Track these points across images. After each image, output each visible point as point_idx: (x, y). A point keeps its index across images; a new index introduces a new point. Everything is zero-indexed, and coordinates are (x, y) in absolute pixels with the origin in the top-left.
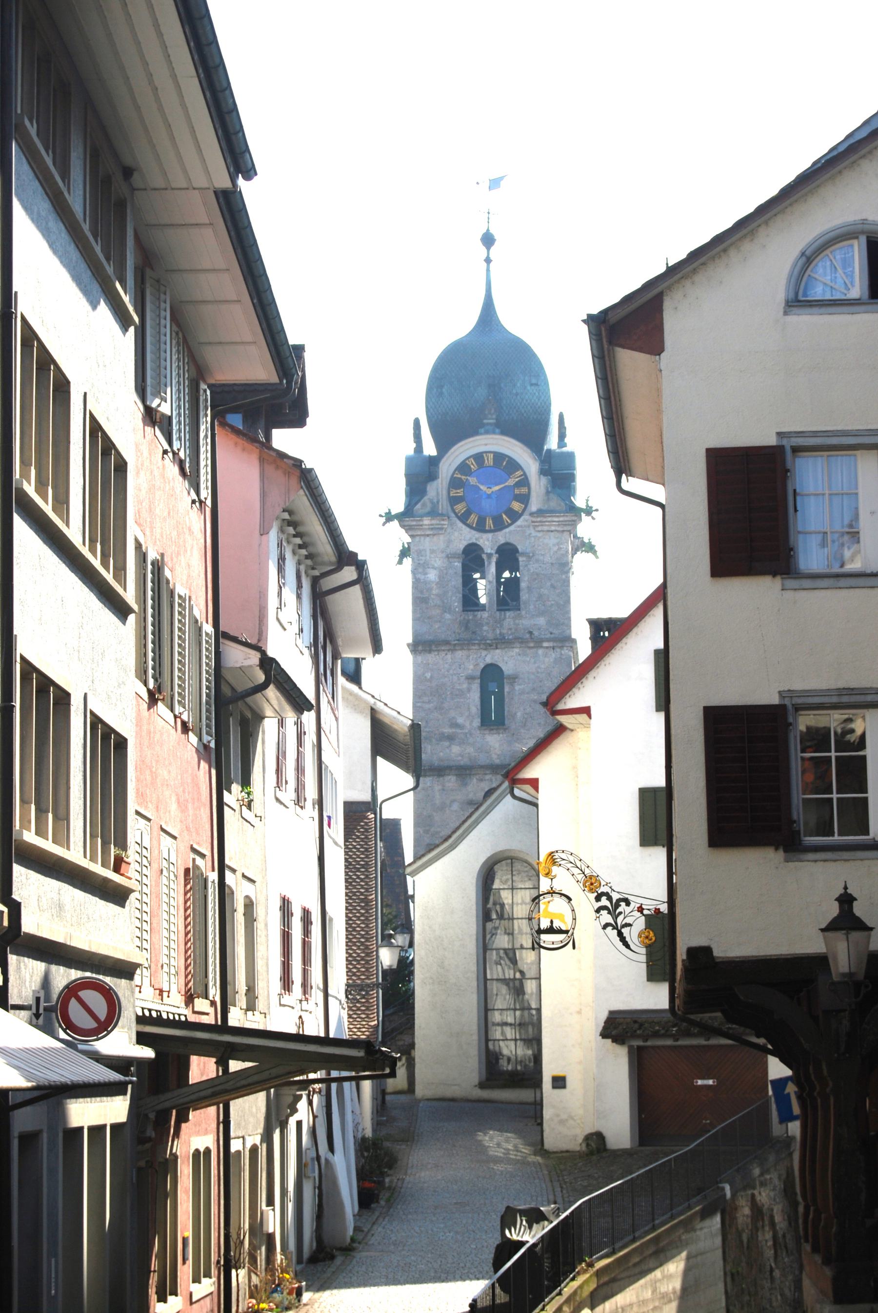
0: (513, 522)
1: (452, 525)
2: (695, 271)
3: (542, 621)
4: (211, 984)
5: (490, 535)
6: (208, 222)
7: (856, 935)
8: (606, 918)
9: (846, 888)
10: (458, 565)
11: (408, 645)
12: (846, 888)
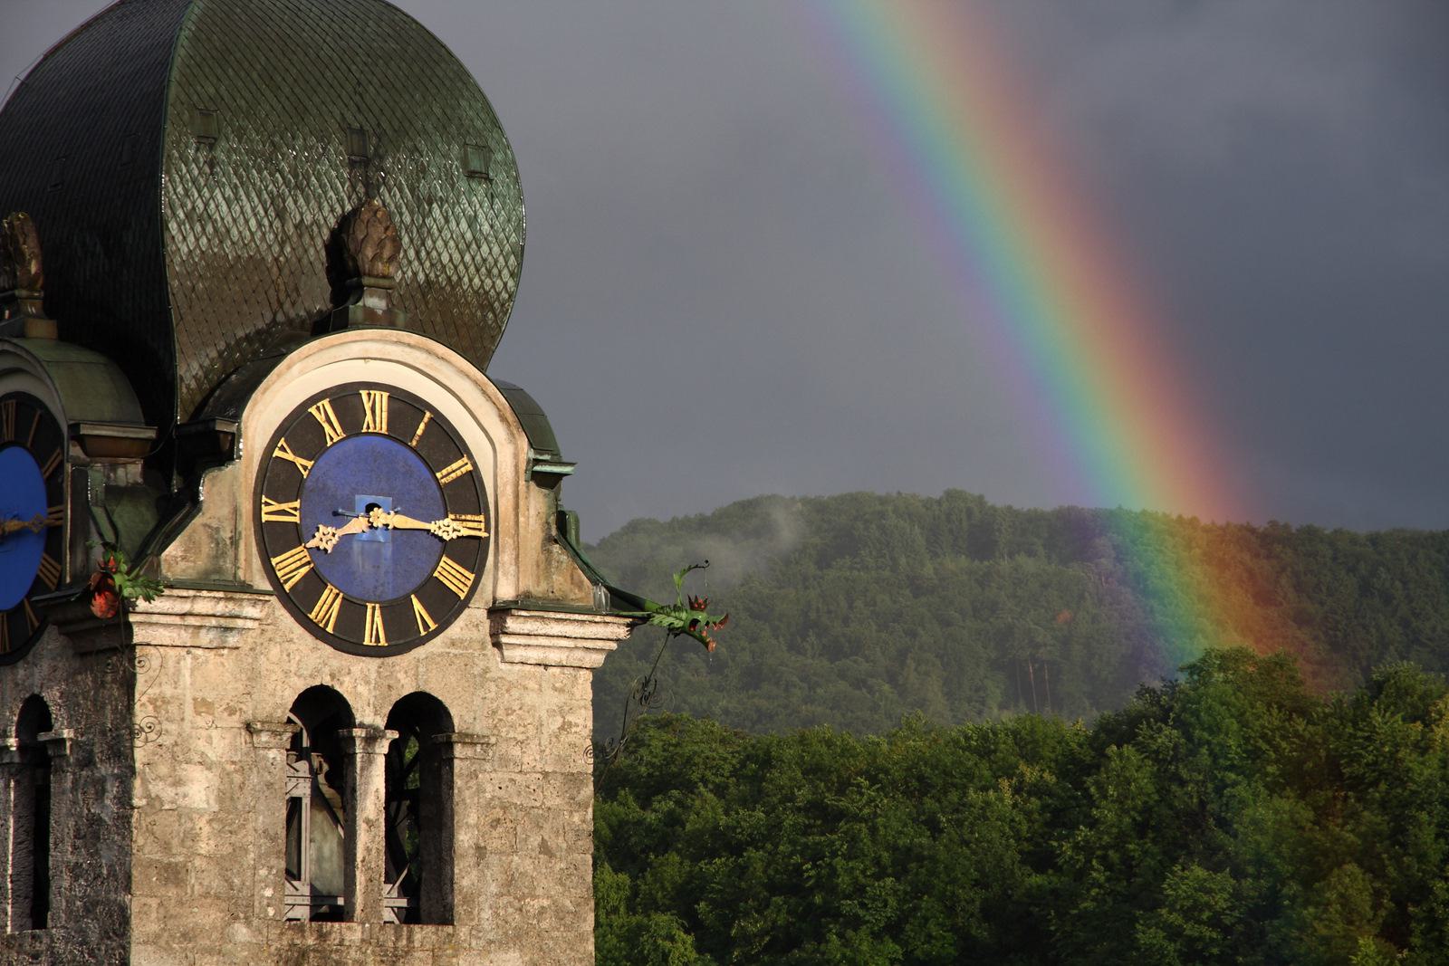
5: (372, 664)
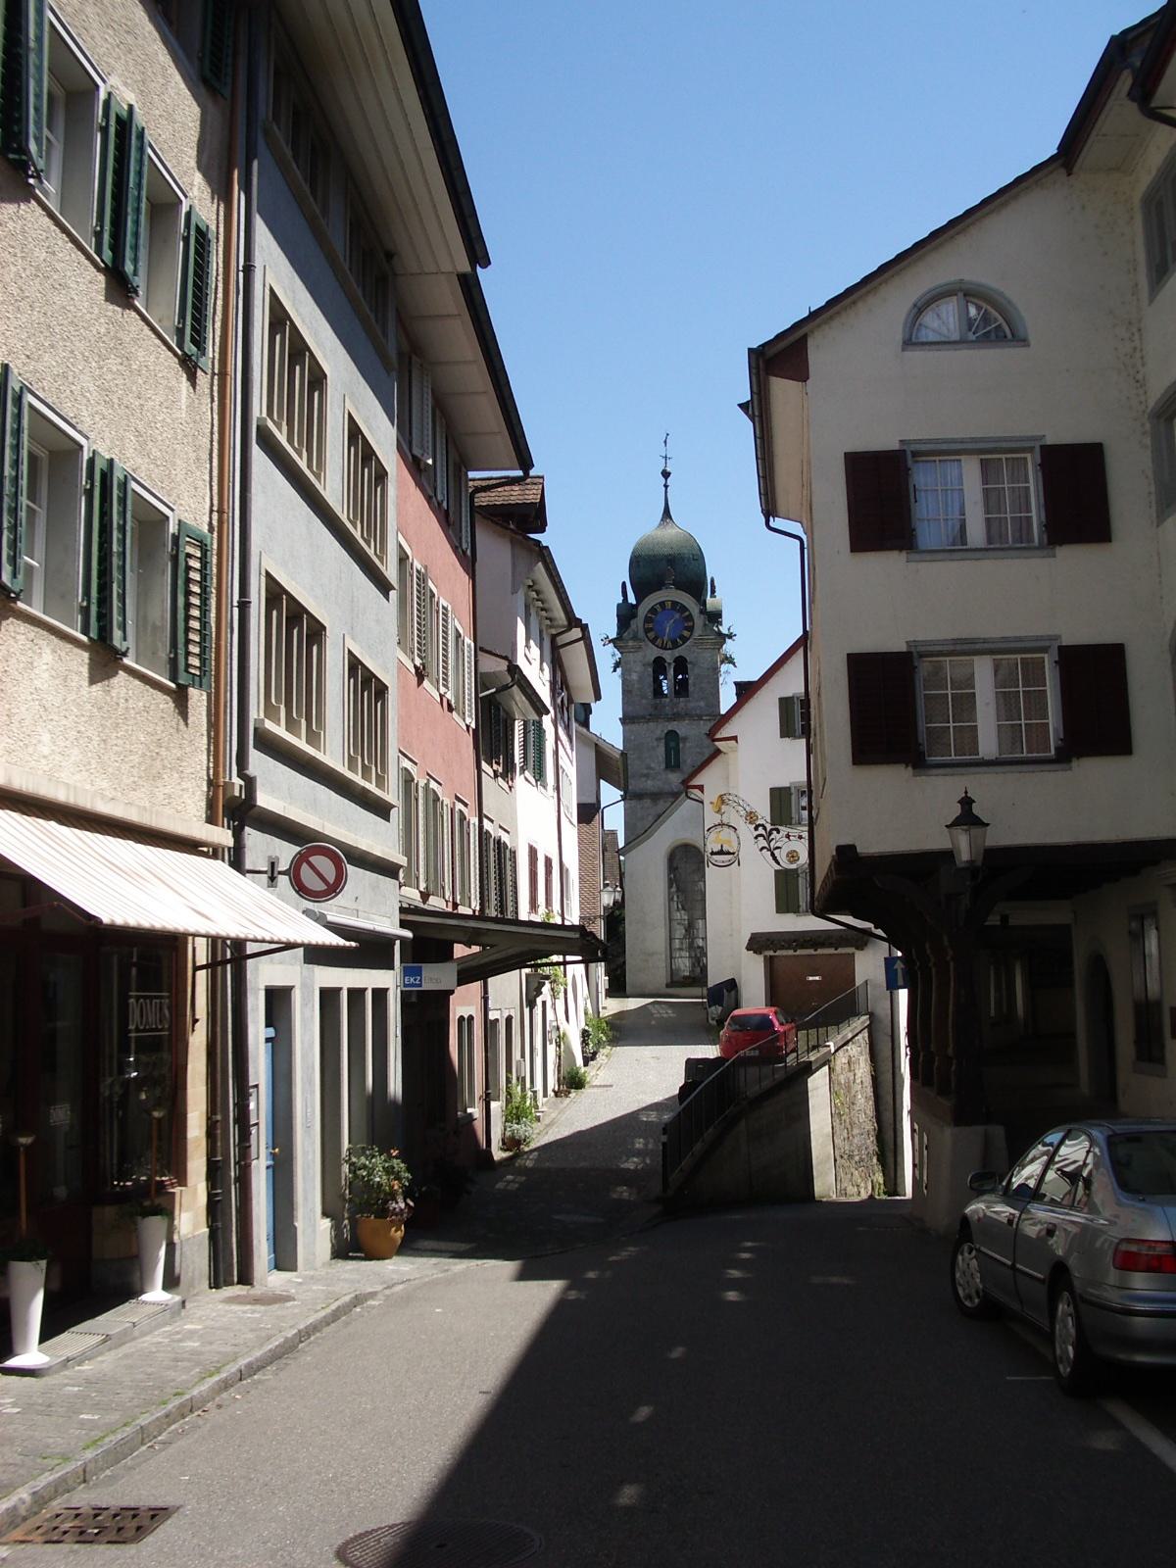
0: (684, 643)
1: (647, 645)
2: (831, 318)
3: (702, 704)
4: (473, 897)
5: (670, 651)
6: (456, 313)
7: (976, 831)
8: (762, 842)
9: (966, 792)
10: (650, 670)
11: (620, 719)
12: (966, 792)
